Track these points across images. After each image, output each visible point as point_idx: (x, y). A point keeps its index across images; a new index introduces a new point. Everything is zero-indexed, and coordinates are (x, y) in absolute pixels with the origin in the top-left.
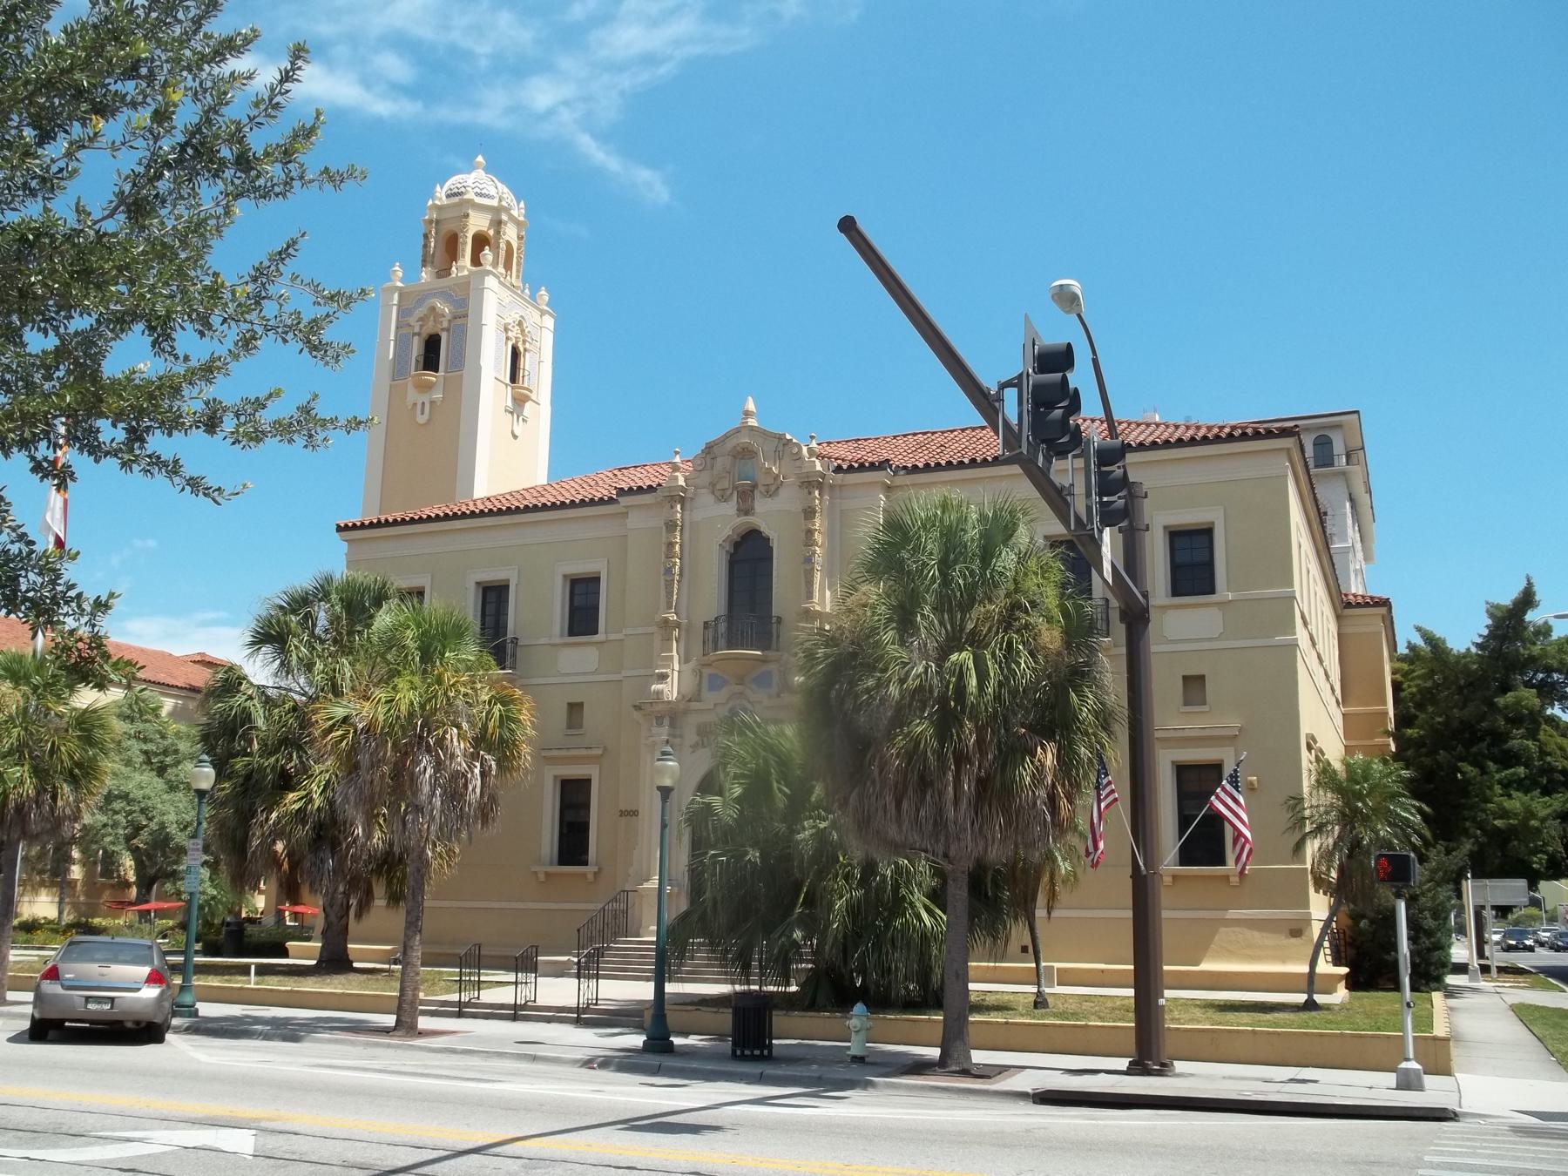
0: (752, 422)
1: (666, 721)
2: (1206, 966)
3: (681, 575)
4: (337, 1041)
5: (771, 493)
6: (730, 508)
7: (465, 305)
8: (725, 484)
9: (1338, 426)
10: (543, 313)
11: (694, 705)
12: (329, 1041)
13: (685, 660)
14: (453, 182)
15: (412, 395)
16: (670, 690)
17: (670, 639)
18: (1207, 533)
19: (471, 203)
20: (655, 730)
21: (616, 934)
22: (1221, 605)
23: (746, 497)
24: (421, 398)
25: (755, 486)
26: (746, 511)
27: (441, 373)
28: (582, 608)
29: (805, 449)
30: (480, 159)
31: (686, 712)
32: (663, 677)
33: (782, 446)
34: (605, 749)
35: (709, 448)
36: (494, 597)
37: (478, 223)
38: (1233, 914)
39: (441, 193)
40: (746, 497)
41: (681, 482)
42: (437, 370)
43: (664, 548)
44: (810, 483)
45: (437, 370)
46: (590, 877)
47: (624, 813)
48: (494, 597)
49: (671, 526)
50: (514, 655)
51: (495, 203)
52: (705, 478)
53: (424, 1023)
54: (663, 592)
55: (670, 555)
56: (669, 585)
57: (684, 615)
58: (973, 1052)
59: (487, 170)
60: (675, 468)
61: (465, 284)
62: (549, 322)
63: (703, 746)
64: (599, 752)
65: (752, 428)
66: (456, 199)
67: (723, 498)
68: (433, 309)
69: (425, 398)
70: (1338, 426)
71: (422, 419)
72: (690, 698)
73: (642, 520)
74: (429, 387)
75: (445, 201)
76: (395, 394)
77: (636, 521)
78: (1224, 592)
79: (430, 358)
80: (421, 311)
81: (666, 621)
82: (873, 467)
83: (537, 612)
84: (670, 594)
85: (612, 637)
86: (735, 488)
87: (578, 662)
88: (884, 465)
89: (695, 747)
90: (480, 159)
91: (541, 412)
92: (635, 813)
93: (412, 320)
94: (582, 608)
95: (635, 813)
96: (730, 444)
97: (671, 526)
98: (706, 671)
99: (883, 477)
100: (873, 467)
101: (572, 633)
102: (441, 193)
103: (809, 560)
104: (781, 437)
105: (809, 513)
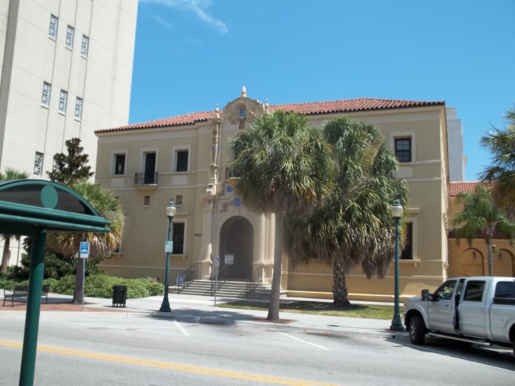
0: (245, 96)
1: (212, 202)
3: (218, 150)
4: (333, 315)
6: (237, 126)
8: (235, 118)
11: (221, 197)
12: (331, 315)
13: (219, 180)
16: (214, 191)
17: (214, 173)
18: (409, 139)
20: (208, 205)
21: (193, 279)
22: (187, 174)
25: (245, 119)
28: (182, 159)
29: (264, 106)
31: (219, 199)
32: (211, 187)
33: (256, 105)
34: (189, 212)
35: (229, 104)
36: (151, 158)
38: (414, 277)
41: (219, 117)
43: (212, 140)
46: (184, 258)
47: (196, 235)
48: (151, 158)
50: (157, 179)
53: (283, 315)
54: (211, 156)
55: (214, 142)
56: (214, 153)
57: (219, 164)
60: (216, 112)
63: (225, 211)
64: (187, 213)
65: (245, 98)
67: (234, 123)
72: (220, 194)
73: (204, 131)
77: (201, 131)
78: (414, 161)
81: (212, 166)
83: (166, 163)
84: (214, 157)
85: (192, 172)
86: (238, 119)
87: (180, 181)
89: (222, 211)
92: (200, 235)
94: (182, 159)
95: (200, 235)
98: (226, 185)
104: (255, 101)
105: (215, 133)
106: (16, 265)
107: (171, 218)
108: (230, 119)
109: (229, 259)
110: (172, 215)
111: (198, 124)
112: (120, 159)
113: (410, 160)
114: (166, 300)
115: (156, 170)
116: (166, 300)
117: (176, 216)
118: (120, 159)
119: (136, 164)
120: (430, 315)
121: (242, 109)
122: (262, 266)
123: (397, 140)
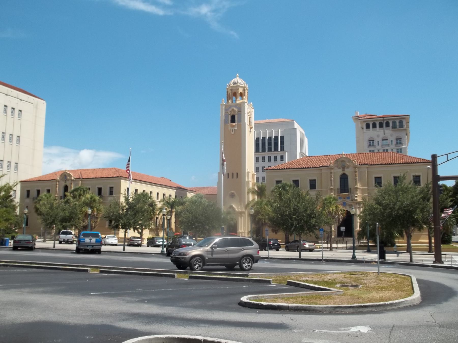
2: (420, 241)
5: (348, 168)
6: (341, 170)
7: (240, 108)
9: (404, 118)
10: (252, 108)
14: (234, 80)
15: (230, 128)
18: (380, 178)
19: (239, 86)
23: (343, 169)
24: (232, 129)
26: (343, 170)
27: (236, 123)
30: (238, 75)
37: (240, 90)
39: (231, 83)
40: (343, 169)
42: (235, 123)
44: (355, 167)
45: (235, 123)
48: (38, 192)
49: (331, 173)
51: (243, 86)
52: (336, 165)
58: (386, 255)
59: (240, 77)
61: (240, 104)
62: (253, 110)
66: (235, 85)
67: (339, 168)
68: (233, 109)
69: (233, 129)
70: (404, 118)
71: (233, 133)
73: (324, 171)
74: (234, 126)
75: (233, 85)
76: (226, 128)
79: (233, 119)
80: (230, 110)
82: (366, 164)
88: (367, 164)
90: (238, 75)
91: (253, 130)
93: (228, 112)
96: (340, 160)
97: (331, 173)
99: (367, 166)
100: (366, 164)
101: (311, 189)
102: (231, 83)
103: (356, 179)
105: (356, 172)
106: (453, 240)
107: (25, 214)
108: (62, 179)
109: (343, 229)
110: (26, 213)
111: (321, 168)
112: (28, 192)
113: (315, 189)
114: (354, 254)
115: (349, 187)
116: (354, 254)
117: (28, 213)
118: (28, 192)
119: (33, 194)
120: (56, 245)
121: (65, 176)
122: (240, 232)
123: (376, 178)
